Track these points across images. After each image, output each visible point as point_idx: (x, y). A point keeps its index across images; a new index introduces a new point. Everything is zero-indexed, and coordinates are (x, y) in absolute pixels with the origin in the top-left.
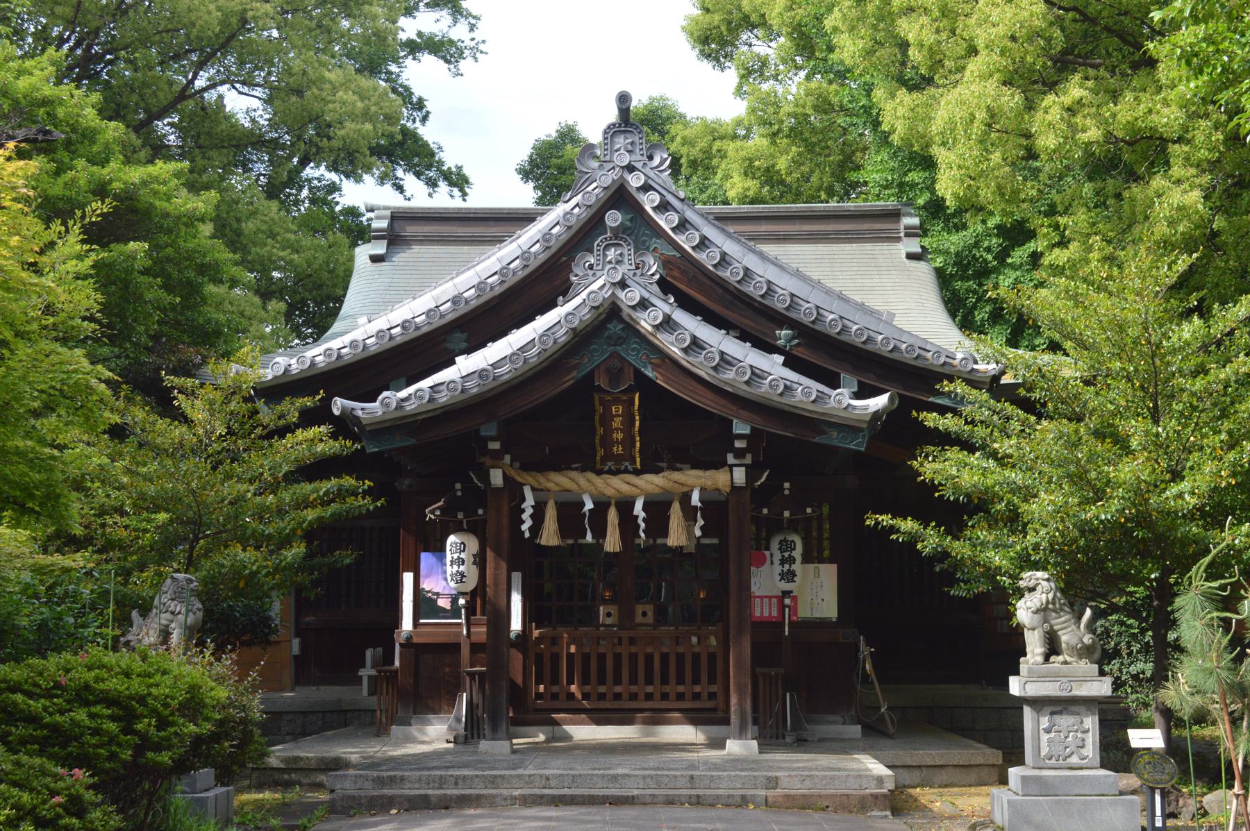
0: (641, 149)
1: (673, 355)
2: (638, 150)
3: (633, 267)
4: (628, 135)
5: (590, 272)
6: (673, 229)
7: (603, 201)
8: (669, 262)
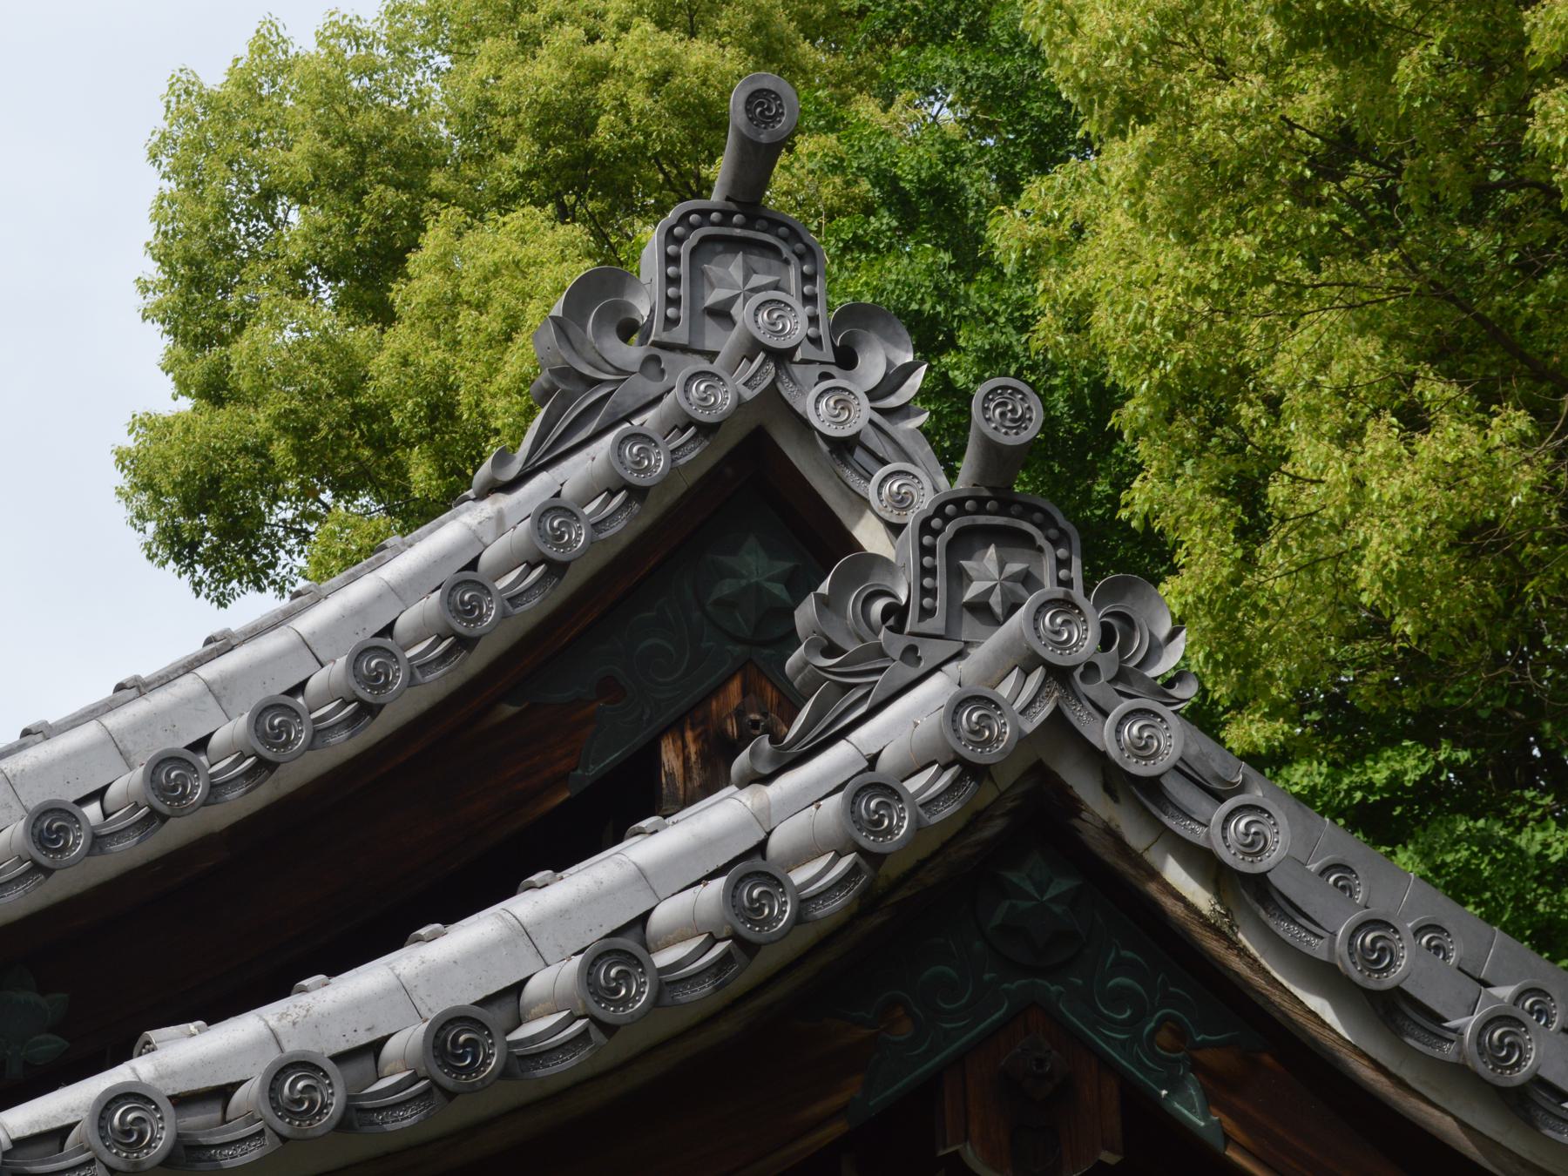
1: (1312, 1027)
5: (895, 644)
7: (692, 477)
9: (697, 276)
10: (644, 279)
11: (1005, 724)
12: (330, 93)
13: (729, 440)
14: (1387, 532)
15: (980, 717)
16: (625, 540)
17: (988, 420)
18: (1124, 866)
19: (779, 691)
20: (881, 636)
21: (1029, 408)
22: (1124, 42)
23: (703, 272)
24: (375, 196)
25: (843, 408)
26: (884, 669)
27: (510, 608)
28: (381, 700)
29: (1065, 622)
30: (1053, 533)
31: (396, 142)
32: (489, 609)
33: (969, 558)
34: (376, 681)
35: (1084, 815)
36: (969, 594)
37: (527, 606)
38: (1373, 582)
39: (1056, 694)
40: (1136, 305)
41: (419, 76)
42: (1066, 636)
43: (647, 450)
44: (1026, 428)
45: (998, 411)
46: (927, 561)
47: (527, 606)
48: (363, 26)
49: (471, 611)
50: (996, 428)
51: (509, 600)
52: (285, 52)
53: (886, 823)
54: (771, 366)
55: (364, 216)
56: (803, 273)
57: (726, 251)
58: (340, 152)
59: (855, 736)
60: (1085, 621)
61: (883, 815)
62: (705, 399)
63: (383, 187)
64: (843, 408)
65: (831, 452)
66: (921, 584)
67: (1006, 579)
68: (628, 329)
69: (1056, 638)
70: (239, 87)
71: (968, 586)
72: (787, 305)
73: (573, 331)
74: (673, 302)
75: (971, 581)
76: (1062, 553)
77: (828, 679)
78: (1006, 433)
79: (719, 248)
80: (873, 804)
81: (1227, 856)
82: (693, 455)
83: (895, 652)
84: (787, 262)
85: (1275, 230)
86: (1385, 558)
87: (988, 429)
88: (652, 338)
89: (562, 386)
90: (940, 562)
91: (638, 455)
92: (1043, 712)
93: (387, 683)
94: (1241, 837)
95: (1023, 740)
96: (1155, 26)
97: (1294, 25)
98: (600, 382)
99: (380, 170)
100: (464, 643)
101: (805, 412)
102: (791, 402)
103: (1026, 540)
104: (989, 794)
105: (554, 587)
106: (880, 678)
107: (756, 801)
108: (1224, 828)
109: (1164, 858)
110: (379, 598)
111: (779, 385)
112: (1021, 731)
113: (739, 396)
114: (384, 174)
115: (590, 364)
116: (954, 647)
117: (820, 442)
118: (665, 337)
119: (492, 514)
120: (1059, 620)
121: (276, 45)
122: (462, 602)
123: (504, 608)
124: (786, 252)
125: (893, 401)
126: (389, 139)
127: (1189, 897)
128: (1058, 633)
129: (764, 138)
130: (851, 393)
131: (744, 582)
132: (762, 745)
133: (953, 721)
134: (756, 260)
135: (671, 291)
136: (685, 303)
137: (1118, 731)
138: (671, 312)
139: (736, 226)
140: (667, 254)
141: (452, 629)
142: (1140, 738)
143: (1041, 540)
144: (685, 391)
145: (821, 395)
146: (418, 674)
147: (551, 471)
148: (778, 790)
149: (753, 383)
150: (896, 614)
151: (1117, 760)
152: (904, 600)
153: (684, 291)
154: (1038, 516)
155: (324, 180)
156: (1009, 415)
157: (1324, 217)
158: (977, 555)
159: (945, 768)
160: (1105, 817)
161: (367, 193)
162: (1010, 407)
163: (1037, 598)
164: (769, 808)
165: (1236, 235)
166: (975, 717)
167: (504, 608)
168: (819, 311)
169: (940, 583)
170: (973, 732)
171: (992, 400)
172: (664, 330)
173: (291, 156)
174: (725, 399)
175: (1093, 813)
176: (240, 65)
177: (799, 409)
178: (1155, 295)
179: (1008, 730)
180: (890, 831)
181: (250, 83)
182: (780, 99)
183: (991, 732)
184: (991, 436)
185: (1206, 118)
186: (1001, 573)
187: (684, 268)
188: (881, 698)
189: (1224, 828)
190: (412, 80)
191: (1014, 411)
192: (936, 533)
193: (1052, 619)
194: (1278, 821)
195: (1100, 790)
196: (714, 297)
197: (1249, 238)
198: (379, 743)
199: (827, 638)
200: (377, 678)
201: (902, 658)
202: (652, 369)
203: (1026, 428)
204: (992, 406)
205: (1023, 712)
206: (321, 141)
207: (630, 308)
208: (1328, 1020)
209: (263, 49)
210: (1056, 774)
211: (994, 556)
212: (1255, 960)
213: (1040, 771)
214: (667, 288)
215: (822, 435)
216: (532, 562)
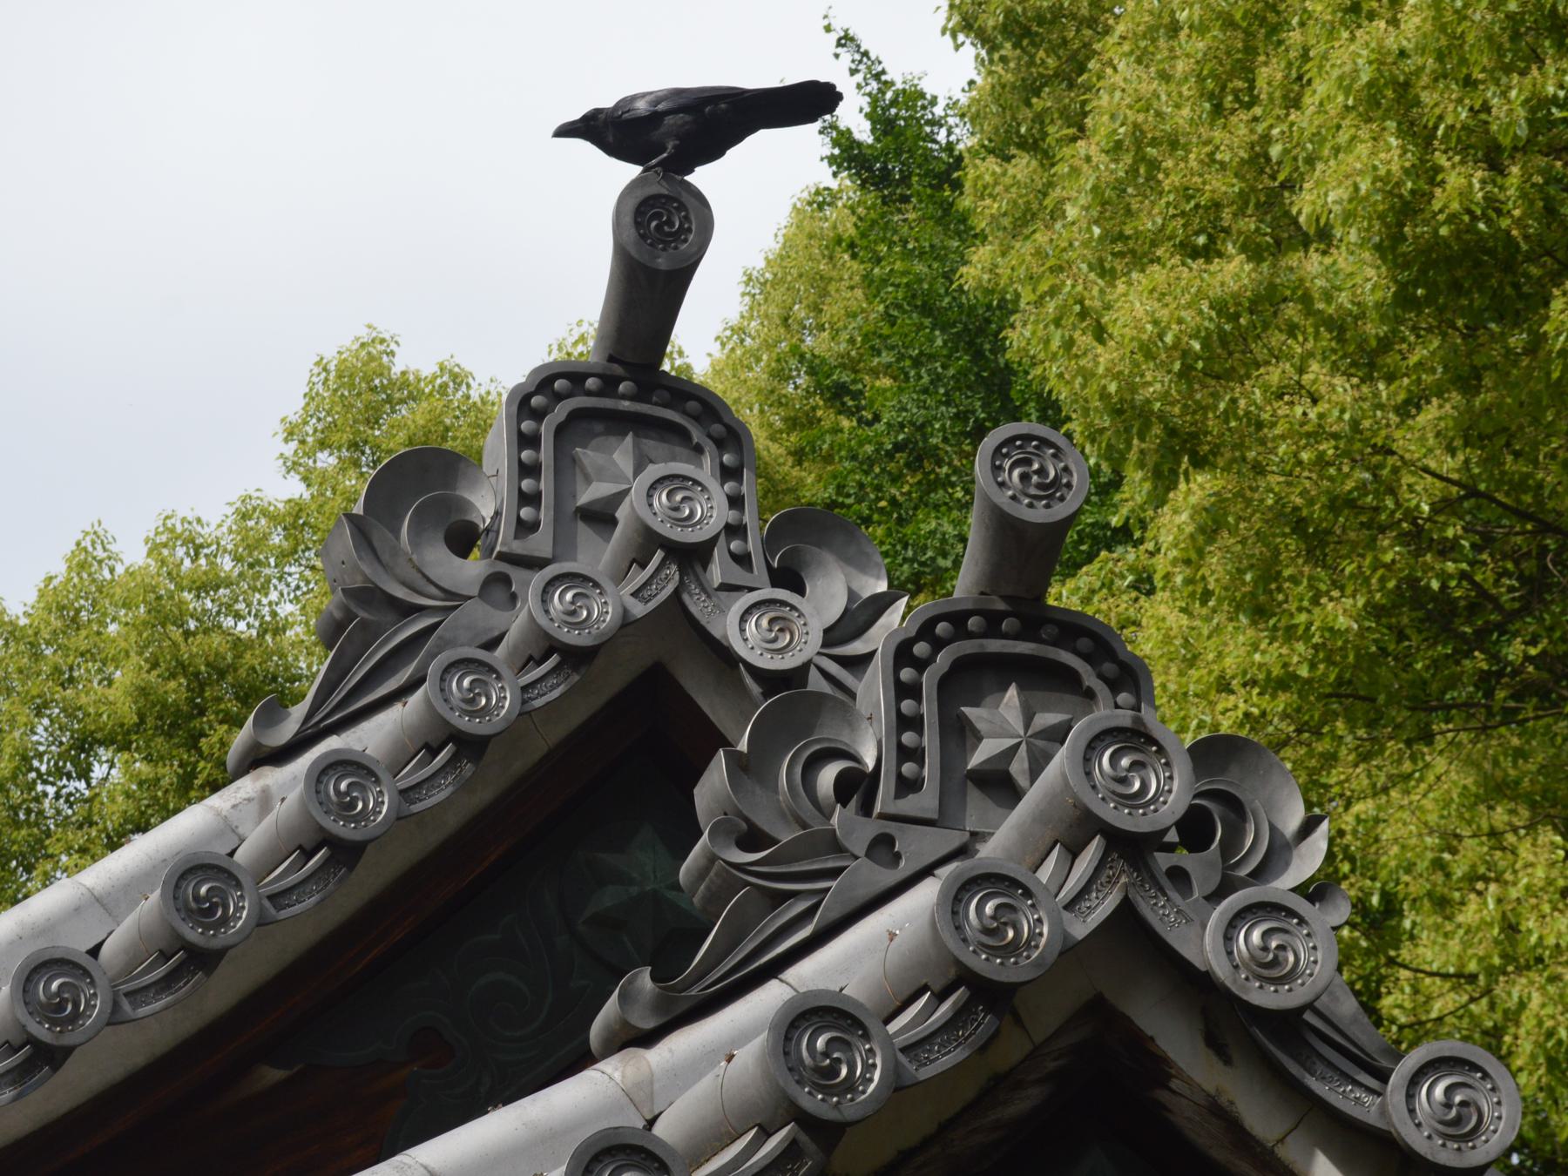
7: (557, 732)
9: (566, 465)
10: (488, 467)
11: (1039, 921)
12: (163, 614)
13: (614, 679)
14: (1551, 989)
15: (998, 907)
16: (452, 821)
17: (1002, 485)
20: (835, 820)
21: (1066, 469)
22: (1169, 339)
23: (574, 461)
24: (215, 739)
25: (781, 630)
26: (841, 870)
27: (273, 911)
28: (67, 1040)
29: (1135, 765)
30: (1109, 668)
31: (242, 673)
32: (239, 909)
33: (976, 704)
34: (56, 1011)
35: (1175, 1084)
36: (976, 759)
37: (297, 908)
38: (1533, 1056)
39: (1124, 879)
40: (1195, 723)
41: (274, 596)
42: (1137, 785)
43: (485, 683)
44: (1062, 499)
45: (1016, 473)
46: (907, 706)
47: (297, 908)
48: (205, 531)
49: (211, 911)
50: (1013, 498)
51: (271, 898)
52: (112, 571)
53: (844, 1071)
54: (673, 570)
55: (202, 764)
56: (722, 465)
57: (608, 432)
58: (172, 684)
59: (792, 974)
60: (1167, 764)
61: (839, 1061)
62: (573, 613)
63: (225, 727)
64: (781, 630)
66: (899, 711)
67: (1035, 736)
68: (463, 539)
69: (1121, 789)
70: (50, 612)
71: (975, 748)
73: (379, 535)
74: (530, 499)
75: (980, 739)
77: (748, 884)
78: (1031, 506)
79: (599, 427)
80: (820, 1043)
81: (1421, 1140)
82: (555, 694)
83: (858, 844)
84: (699, 450)
85: (1382, 588)
86: (1549, 1023)
87: (1003, 499)
88: (498, 548)
89: (362, 614)
90: (928, 708)
91: (470, 690)
92: (1104, 906)
93: (76, 1016)
94: (1440, 1110)
95: (1071, 952)
96: (1211, 319)
97: (1406, 266)
98: (421, 609)
99: (222, 706)
100: (200, 960)
101: (726, 637)
102: (703, 622)
104: (1013, 1050)
105: (341, 880)
106: (834, 884)
107: (630, 1071)
108: (1410, 1096)
109: (1310, 1158)
110: (77, 911)
111: (686, 597)
112: (1066, 936)
113: (626, 611)
114: (227, 712)
115: (405, 584)
116: (954, 839)
117: (748, 680)
118: (518, 547)
119: (254, 795)
120: (1125, 762)
121: (100, 562)
122: (197, 898)
123: (262, 908)
124: (697, 435)
125: (857, 648)
126: (234, 668)
128: (1124, 781)
129: (662, 263)
130: (793, 608)
131: (634, 890)
132: (639, 983)
133: (954, 913)
134: (650, 445)
135: (527, 484)
136: (547, 500)
137: (1228, 938)
138: (526, 513)
139: (624, 397)
140: (520, 433)
141: (178, 937)
142: (1265, 949)
143: (1090, 679)
144: (544, 601)
145: (748, 612)
146: (126, 1005)
147: (344, 735)
148: (666, 1055)
149: (646, 594)
150: (857, 786)
151: (1228, 983)
152: (870, 763)
153: (546, 484)
154: (1084, 643)
155: (150, 722)
156: (1035, 478)
157: (1450, 566)
158: (989, 700)
159: (941, 997)
160: (1210, 1087)
161: (206, 736)
162: (1036, 466)
163: (1090, 724)
164: (652, 1083)
165: (1331, 599)
166: (989, 908)
167: (262, 908)
168: (747, 519)
169: (930, 740)
170: (987, 931)
171: (1007, 456)
172: (516, 537)
173: (112, 694)
174: (602, 614)
175: (1189, 1081)
176: (55, 582)
177: (716, 633)
178: (1220, 707)
179: (1045, 930)
180: (850, 1085)
181: (64, 607)
182: (686, 210)
183: (1018, 932)
184: (1006, 508)
185: (1283, 437)
186: (1027, 726)
187: (546, 454)
188: (835, 915)
189: (1410, 1096)
190: (265, 601)
191: (1042, 472)
192: (921, 665)
193: (1114, 759)
194: (1500, 1083)
195: (1201, 1044)
196: (588, 495)
197: (1349, 602)
198: (65, 1116)
199: (747, 820)
200: (61, 1007)
201: (868, 855)
202: (499, 593)
203: (1062, 499)
204: (1007, 464)
205: (1069, 906)
206: (148, 672)
207: (466, 505)
209: (83, 566)
210: (1129, 1019)
211: (1016, 701)
213: (1099, 1011)
214: (520, 452)
215: (749, 667)
216: (308, 847)
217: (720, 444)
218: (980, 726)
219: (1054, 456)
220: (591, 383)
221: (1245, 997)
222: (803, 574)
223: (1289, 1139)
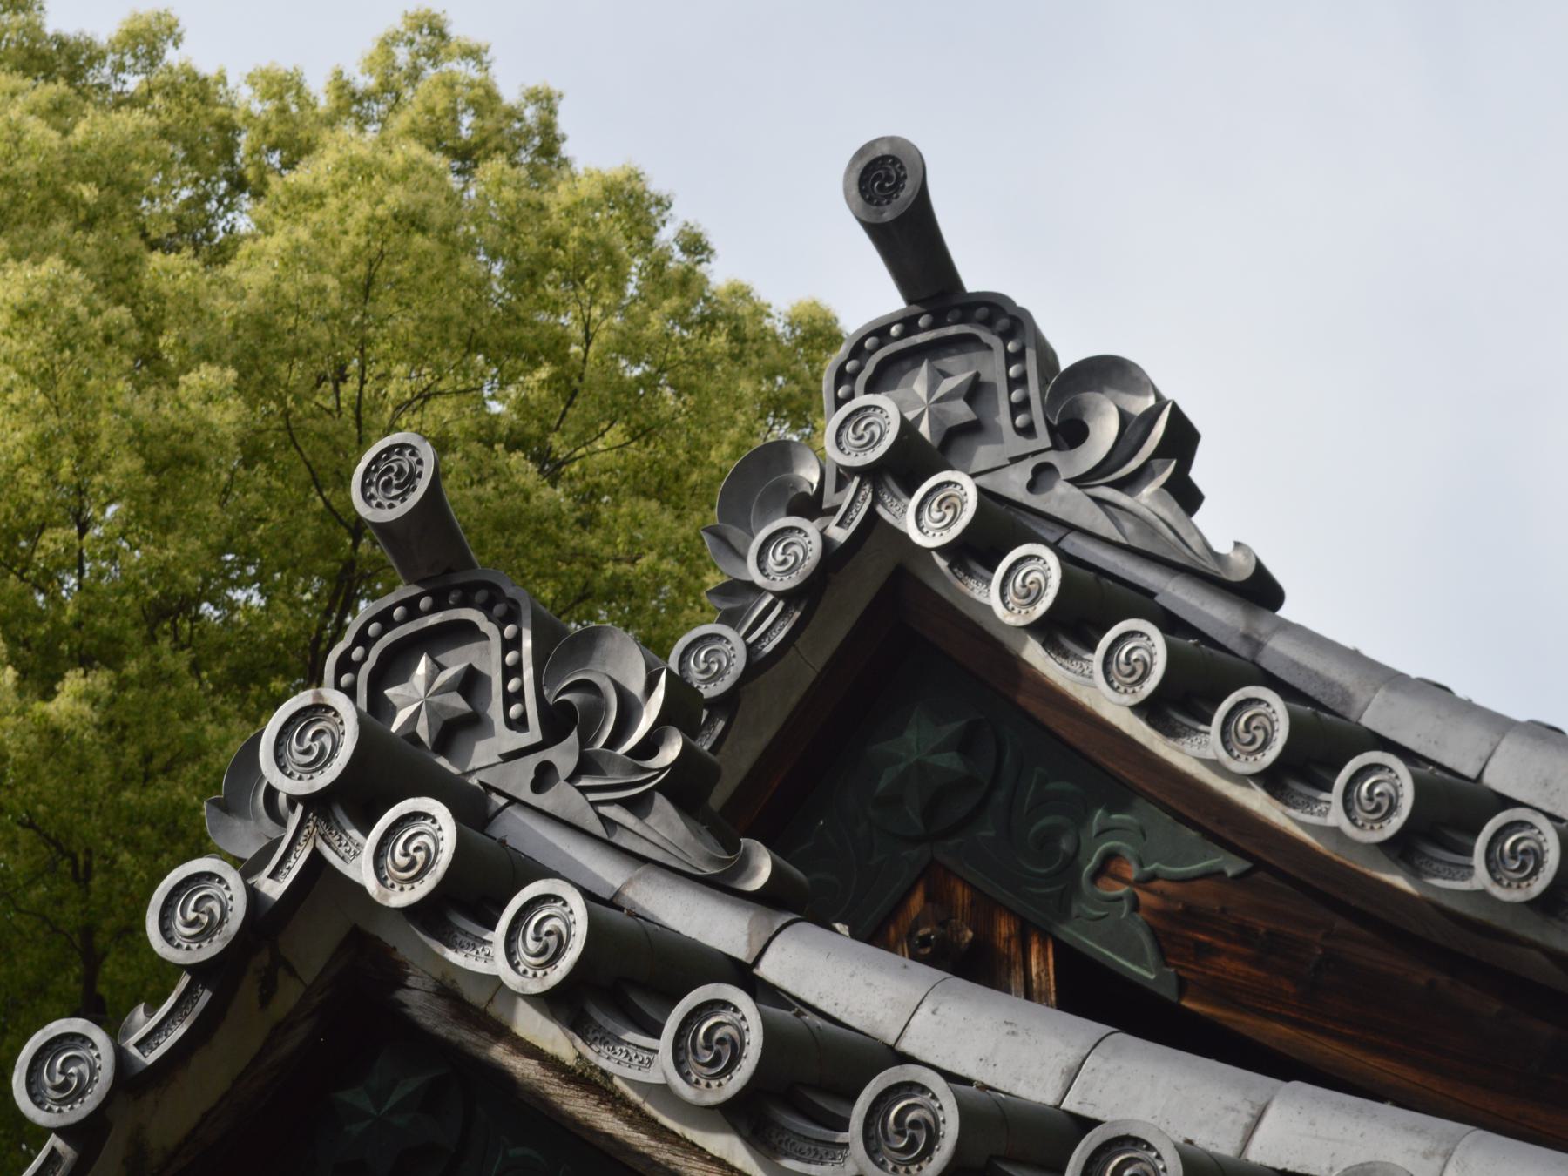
0: (1023, 406)
2: (1004, 418)
3: (534, 735)
4: (949, 363)
6: (1149, 709)
8: (1190, 916)
18: (463, 1035)
19: (972, 887)
65: (951, 567)
72: (876, 407)
76: (510, 630)
103: (467, 632)
111: (880, 509)
124: (985, 335)
127: (549, 1048)
131: (901, 767)
208: (738, 1164)
210: (378, 939)
212: (638, 1109)
217: (1006, 336)
218: (396, 702)
219: (411, 454)
220: (894, 330)
221: (386, 904)
222: (1085, 419)
223: (496, 997)
